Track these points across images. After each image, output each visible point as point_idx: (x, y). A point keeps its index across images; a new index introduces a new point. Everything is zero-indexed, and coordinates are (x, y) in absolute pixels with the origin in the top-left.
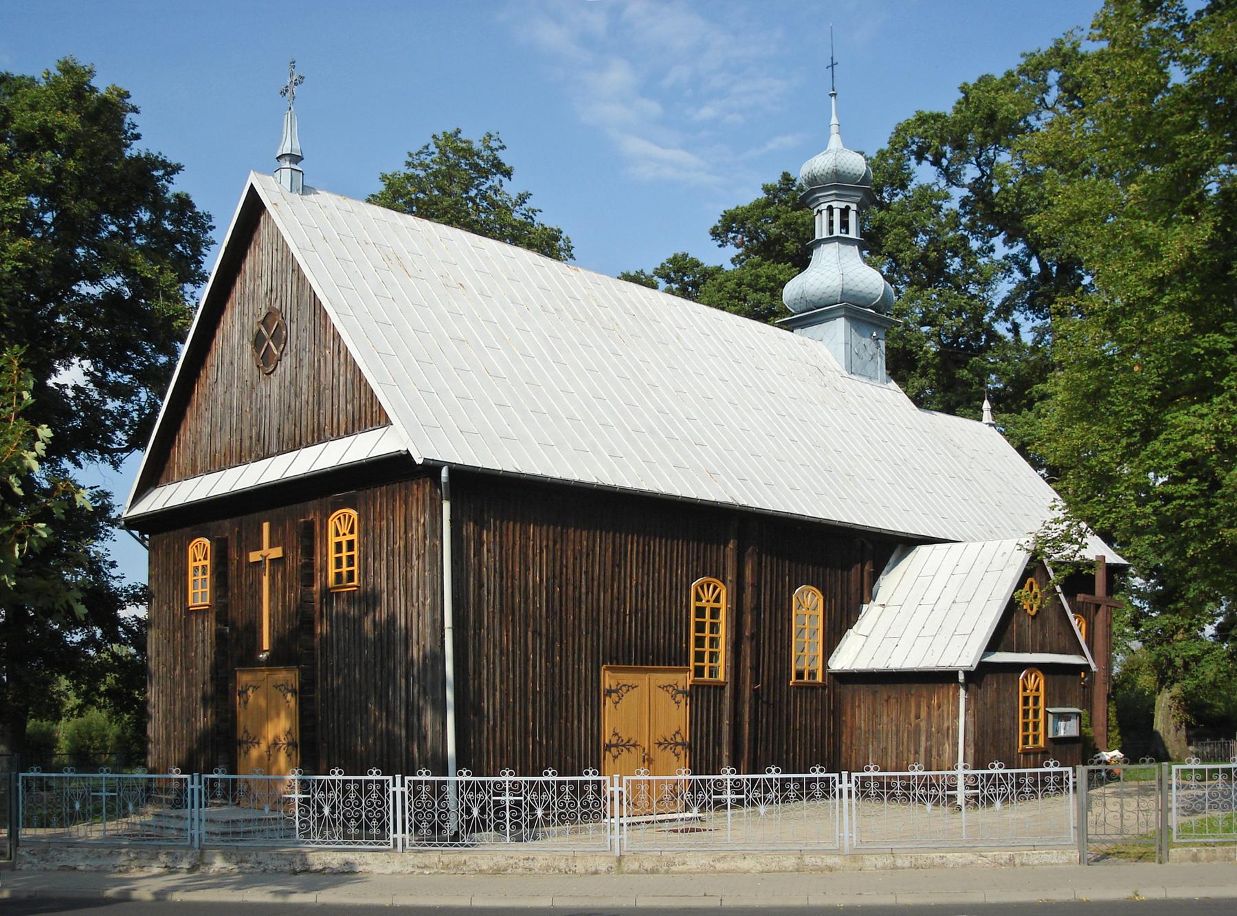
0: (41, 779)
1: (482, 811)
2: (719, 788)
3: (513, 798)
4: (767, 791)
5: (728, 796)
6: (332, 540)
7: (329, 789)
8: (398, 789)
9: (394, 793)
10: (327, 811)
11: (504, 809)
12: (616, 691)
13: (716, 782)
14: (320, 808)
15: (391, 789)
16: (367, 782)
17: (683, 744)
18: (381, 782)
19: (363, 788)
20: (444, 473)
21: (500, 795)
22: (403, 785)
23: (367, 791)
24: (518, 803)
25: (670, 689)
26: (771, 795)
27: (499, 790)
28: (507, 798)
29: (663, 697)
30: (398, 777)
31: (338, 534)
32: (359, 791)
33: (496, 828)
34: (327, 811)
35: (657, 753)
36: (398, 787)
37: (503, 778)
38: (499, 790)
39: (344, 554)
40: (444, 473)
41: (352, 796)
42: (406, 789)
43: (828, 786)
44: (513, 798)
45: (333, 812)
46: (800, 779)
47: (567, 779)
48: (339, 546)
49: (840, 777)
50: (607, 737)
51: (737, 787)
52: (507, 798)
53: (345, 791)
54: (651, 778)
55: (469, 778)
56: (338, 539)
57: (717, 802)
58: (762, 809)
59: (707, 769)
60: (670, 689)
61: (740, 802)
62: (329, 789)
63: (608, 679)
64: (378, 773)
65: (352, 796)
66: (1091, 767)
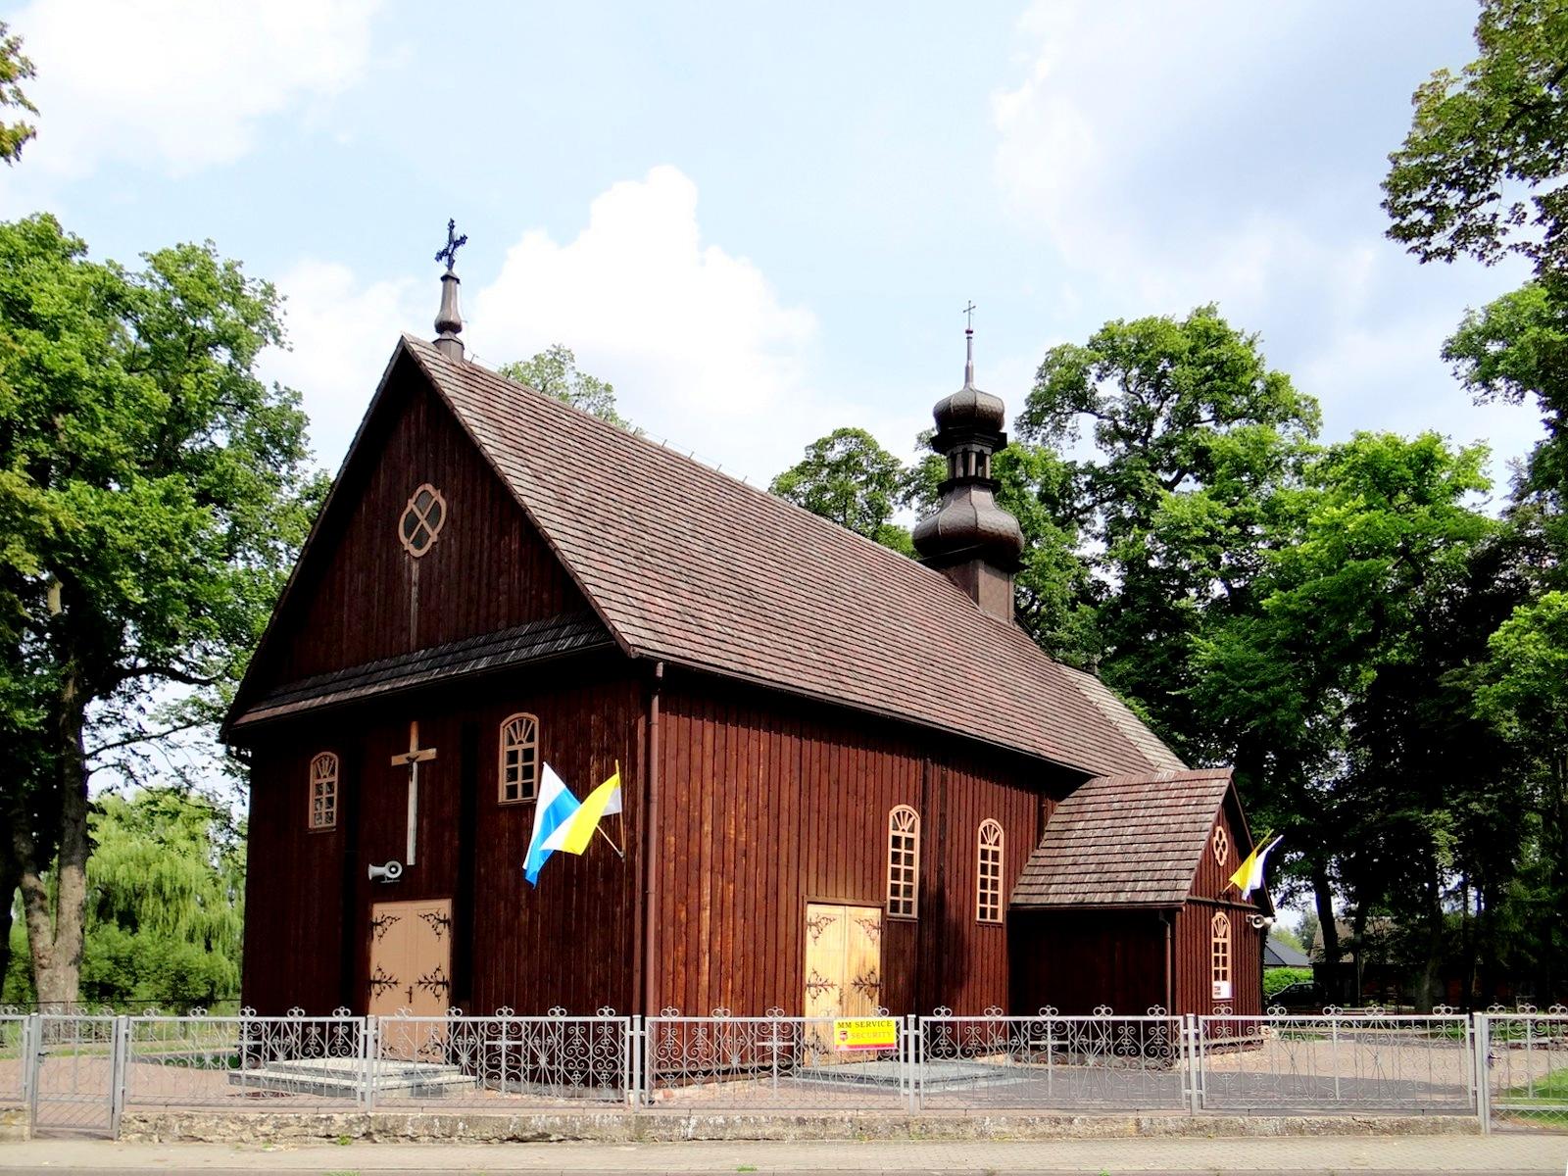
0: (952, 1024)
1: (473, 1056)
2: (1038, 1031)
3: (782, 1044)
4: (1096, 1036)
5: (1050, 1041)
6: (504, 749)
7: (547, 1034)
8: (637, 1032)
9: (631, 1038)
10: (543, 1061)
11: (500, 1055)
12: (816, 924)
13: (490, 1024)
14: (534, 1059)
15: (628, 1033)
16: (334, 1025)
17: (443, 983)
18: (614, 1025)
19: (593, 1033)
20: (660, 667)
21: (495, 1039)
22: (917, 1028)
23: (332, 1035)
24: (517, 1049)
25: (431, 918)
26: (1102, 1041)
27: (494, 1030)
28: (504, 1043)
29: (426, 927)
30: (637, 1018)
31: (511, 742)
32: (586, 1036)
33: (490, 1076)
34: (543, 1061)
35: (418, 991)
36: (633, 1029)
37: (1042, 1018)
38: (494, 1030)
39: (520, 765)
40: (660, 667)
41: (313, 1042)
42: (921, 1033)
43: (616, 1030)
44: (782, 1044)
45: (551, 1062)
46: (1138, 1022)
47: (314, 1019)
48: (513, 757)
49: (1471, 1018)
50: (809, 976)
51: (1060, 1030)
52: (504, 1043)
53: (305, 1035)
54: (954, 1019)
55: (1000, 1018)
56: (512, 748)
57: (1035, 1048)
58: (1091, 1059)
59: (964, 1009)
60: (431, 918)
61: (1063, 1049)
62: (470, 1033)
63: (813, 912)
64: (611, 1013)
65: (313, 1042)
66: (1492, 1015)
